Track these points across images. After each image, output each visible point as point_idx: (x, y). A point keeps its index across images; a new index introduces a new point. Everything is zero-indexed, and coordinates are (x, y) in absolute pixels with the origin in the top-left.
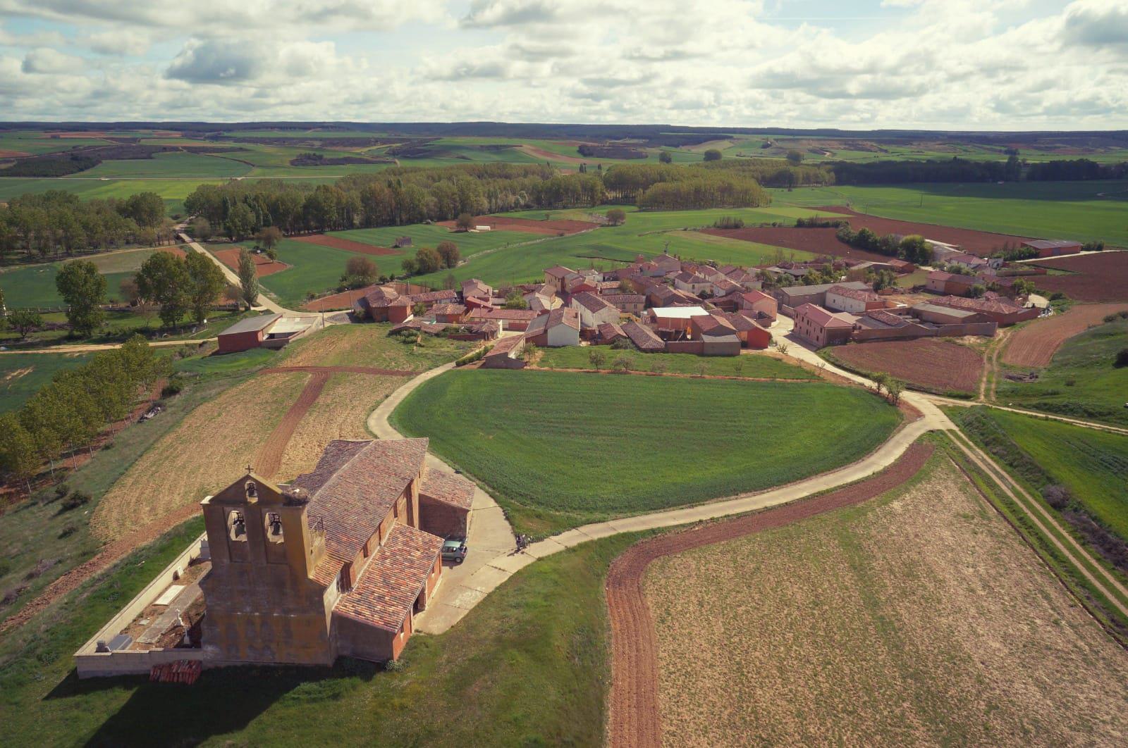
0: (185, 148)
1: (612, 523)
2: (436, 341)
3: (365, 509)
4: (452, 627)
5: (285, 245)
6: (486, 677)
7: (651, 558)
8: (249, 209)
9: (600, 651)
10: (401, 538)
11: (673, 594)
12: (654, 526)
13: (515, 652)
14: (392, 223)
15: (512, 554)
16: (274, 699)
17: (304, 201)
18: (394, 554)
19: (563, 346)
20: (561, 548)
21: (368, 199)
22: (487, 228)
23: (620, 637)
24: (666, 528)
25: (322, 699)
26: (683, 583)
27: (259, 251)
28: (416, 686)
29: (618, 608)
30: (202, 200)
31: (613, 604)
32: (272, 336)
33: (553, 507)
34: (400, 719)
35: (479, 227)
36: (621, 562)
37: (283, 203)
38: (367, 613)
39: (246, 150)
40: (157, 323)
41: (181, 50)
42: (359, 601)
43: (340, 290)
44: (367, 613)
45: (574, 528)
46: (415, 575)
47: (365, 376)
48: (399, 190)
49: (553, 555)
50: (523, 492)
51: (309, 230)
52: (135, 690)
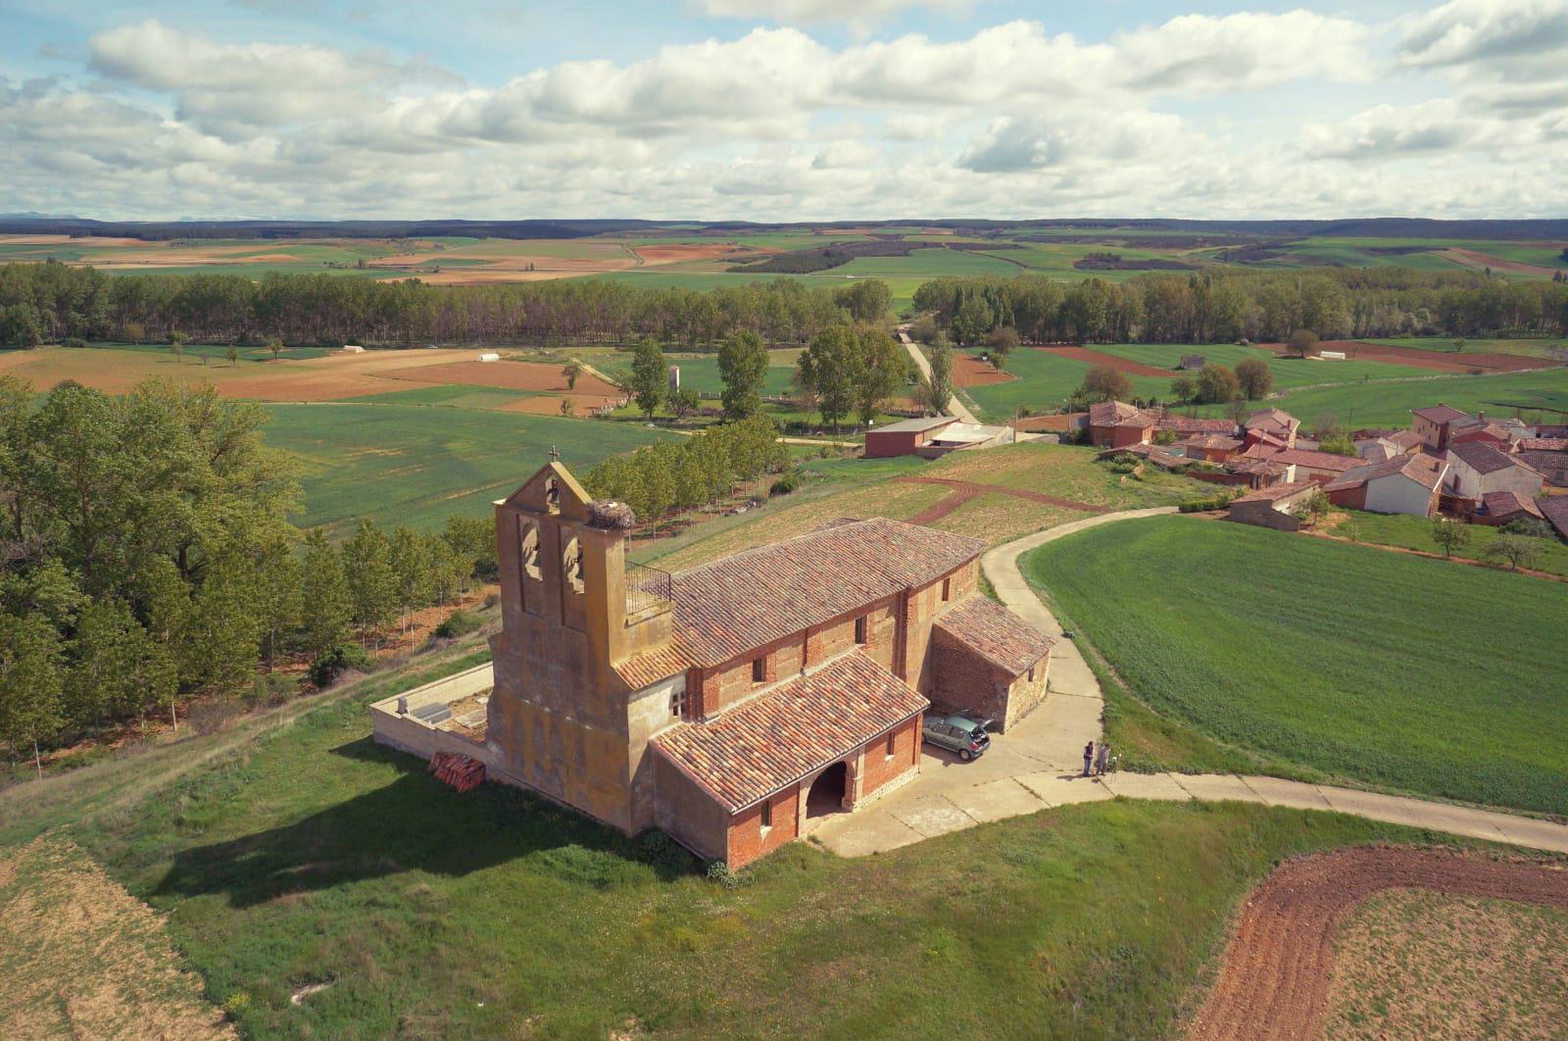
0: (948, 244)
1: (1326, 791)
2: (1167, 476)
3: (790, 603)
4: (875, 853)
5: (1020, 354)
6: (864, 960)
7: (1392, 882)
8: (986, 304)
9: (1152, 1016)
10: (849, 675)
11: (1415, 973)
12: (1432, 825)
13: (949, 937)
14: (1187, 339)
15: (1069, 778)
16: (521, 853)
17: (1064, 300)
18: (818, 694)
19: (1395, 514)
20: (1185, 796)
21: (1155, 302)
22: (1341, 355)
23: (1225, 1008)
24: (1464, 839)
25: (580, 880)
26: (1458, 963)
27: (985, 358)
28: (735, 920)
29: (1254, 948)
30: (935, 293)
31: (1247, 940)
32: (937, 443)
33: (1218, 733)
34: (668, 965)
35: (1326, 354)
36: (1311, 868)
37: (1033, 300)
38: (705, 764)
39: (1021, 247)
40: (816, 419)
41: (984, 132)
42: (706, 741)
43: (1067, 411)
44: (705, 764)
45: (1234, 772)
46: (834, 736)
47: (1025, 501)
48: (1205, 292)
49: (1157, 802)
50: (1171, 693)
51: (1063, 339)
52: (405, 774)
